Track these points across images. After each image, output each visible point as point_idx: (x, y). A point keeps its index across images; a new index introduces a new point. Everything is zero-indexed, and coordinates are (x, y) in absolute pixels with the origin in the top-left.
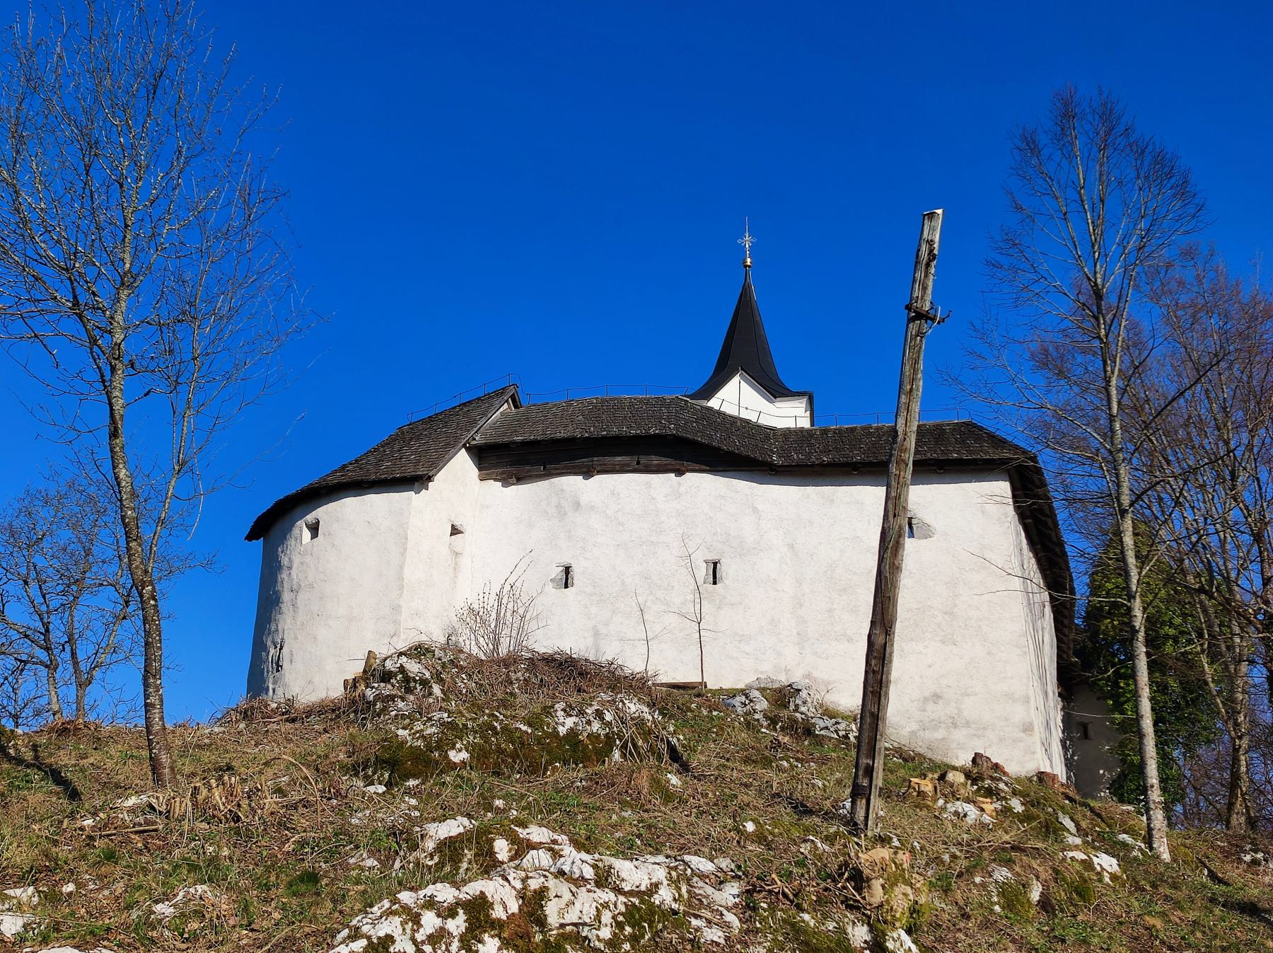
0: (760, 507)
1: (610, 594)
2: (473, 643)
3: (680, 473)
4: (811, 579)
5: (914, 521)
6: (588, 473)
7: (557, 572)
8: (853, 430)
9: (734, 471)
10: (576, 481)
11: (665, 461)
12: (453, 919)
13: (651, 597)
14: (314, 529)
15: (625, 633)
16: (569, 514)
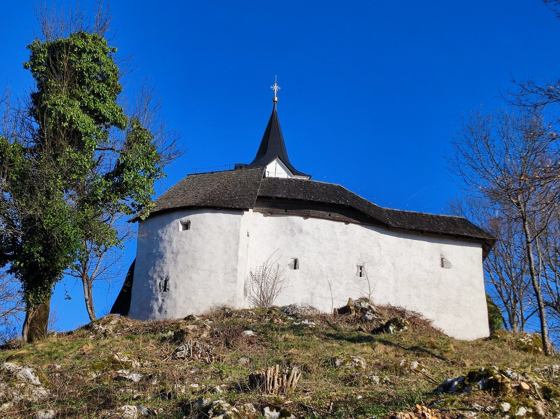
0: (381, 244)
1: (315, 275)
2: (251, 289)
3: (347, 223)
4: (401, 280)
5: (444, 260)
6: (306, 216)
7: (292, 261)
8: (415, 214)
9: (376, 226)
10: (301, 219)
11: (342, 217)
12: (270, 411)
13: (333, 279)
14: (186, 226)
15: (322, 294)
16: (297, 234)
